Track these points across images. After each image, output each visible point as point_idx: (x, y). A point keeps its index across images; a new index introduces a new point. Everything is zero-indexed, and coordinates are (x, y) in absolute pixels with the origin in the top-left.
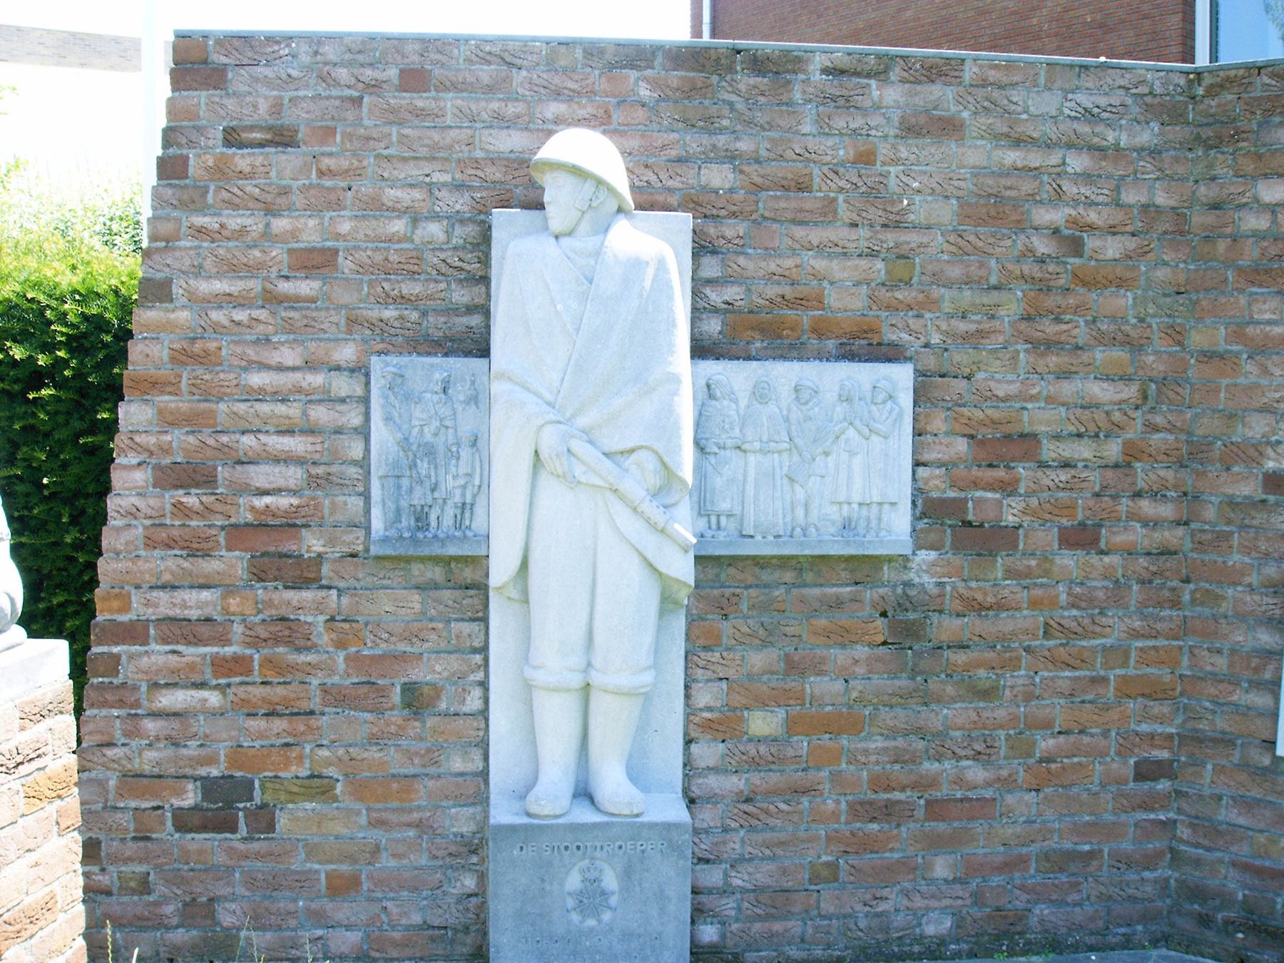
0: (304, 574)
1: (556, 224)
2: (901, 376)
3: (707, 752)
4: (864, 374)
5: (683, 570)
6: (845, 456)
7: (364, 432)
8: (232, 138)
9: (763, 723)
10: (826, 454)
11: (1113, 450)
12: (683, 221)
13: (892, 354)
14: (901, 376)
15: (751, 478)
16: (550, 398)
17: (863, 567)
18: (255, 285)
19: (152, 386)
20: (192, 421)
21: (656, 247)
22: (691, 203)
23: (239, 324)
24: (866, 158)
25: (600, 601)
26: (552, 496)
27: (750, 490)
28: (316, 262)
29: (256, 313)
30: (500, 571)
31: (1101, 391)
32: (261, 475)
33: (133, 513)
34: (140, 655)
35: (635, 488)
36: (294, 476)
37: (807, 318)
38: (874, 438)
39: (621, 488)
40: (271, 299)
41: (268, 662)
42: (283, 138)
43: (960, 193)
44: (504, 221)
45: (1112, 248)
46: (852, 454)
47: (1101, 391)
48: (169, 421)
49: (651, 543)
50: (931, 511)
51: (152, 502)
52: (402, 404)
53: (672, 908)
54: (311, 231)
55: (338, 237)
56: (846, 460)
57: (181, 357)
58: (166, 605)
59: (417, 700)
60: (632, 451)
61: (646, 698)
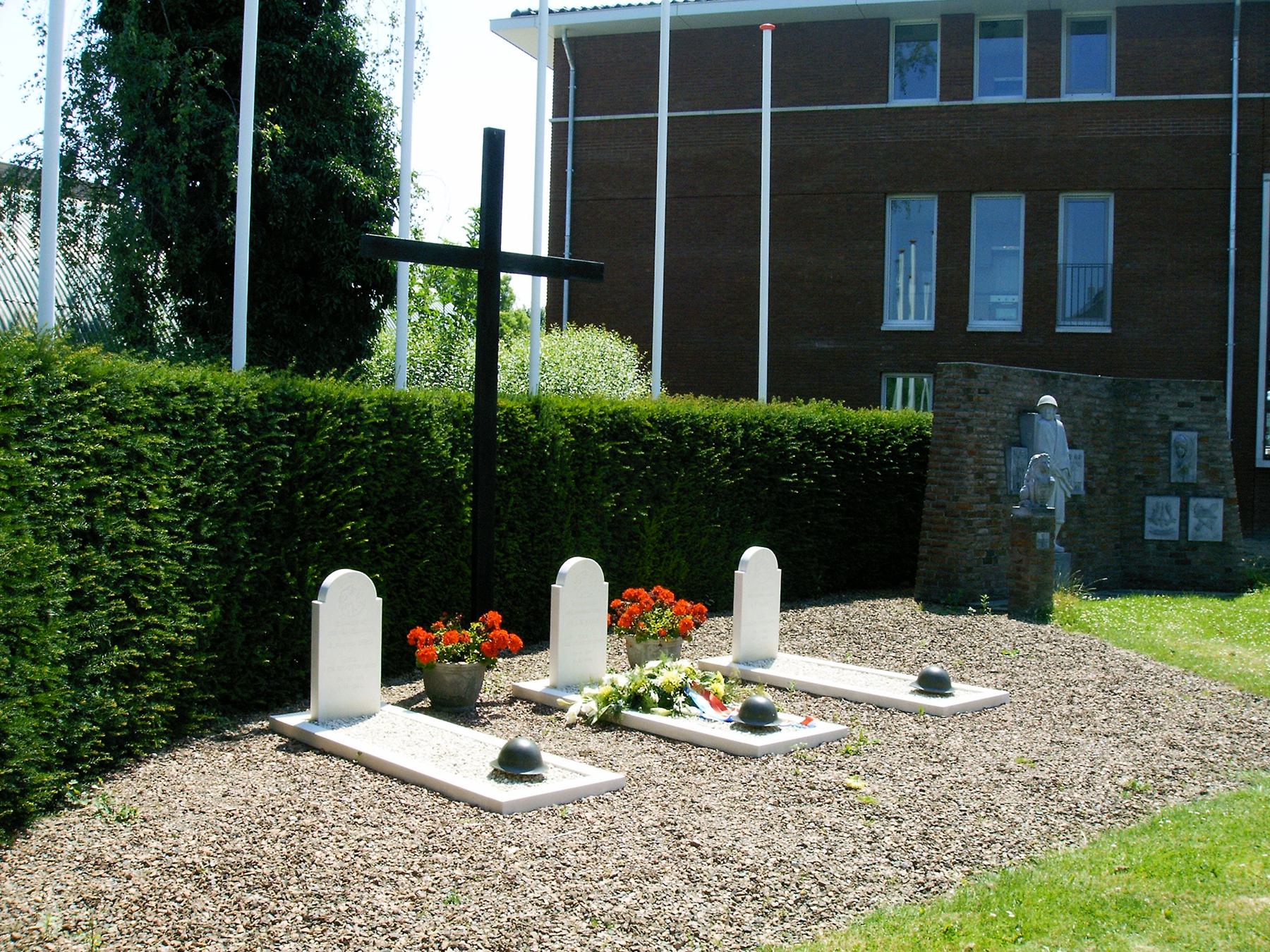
42: (987, 392)
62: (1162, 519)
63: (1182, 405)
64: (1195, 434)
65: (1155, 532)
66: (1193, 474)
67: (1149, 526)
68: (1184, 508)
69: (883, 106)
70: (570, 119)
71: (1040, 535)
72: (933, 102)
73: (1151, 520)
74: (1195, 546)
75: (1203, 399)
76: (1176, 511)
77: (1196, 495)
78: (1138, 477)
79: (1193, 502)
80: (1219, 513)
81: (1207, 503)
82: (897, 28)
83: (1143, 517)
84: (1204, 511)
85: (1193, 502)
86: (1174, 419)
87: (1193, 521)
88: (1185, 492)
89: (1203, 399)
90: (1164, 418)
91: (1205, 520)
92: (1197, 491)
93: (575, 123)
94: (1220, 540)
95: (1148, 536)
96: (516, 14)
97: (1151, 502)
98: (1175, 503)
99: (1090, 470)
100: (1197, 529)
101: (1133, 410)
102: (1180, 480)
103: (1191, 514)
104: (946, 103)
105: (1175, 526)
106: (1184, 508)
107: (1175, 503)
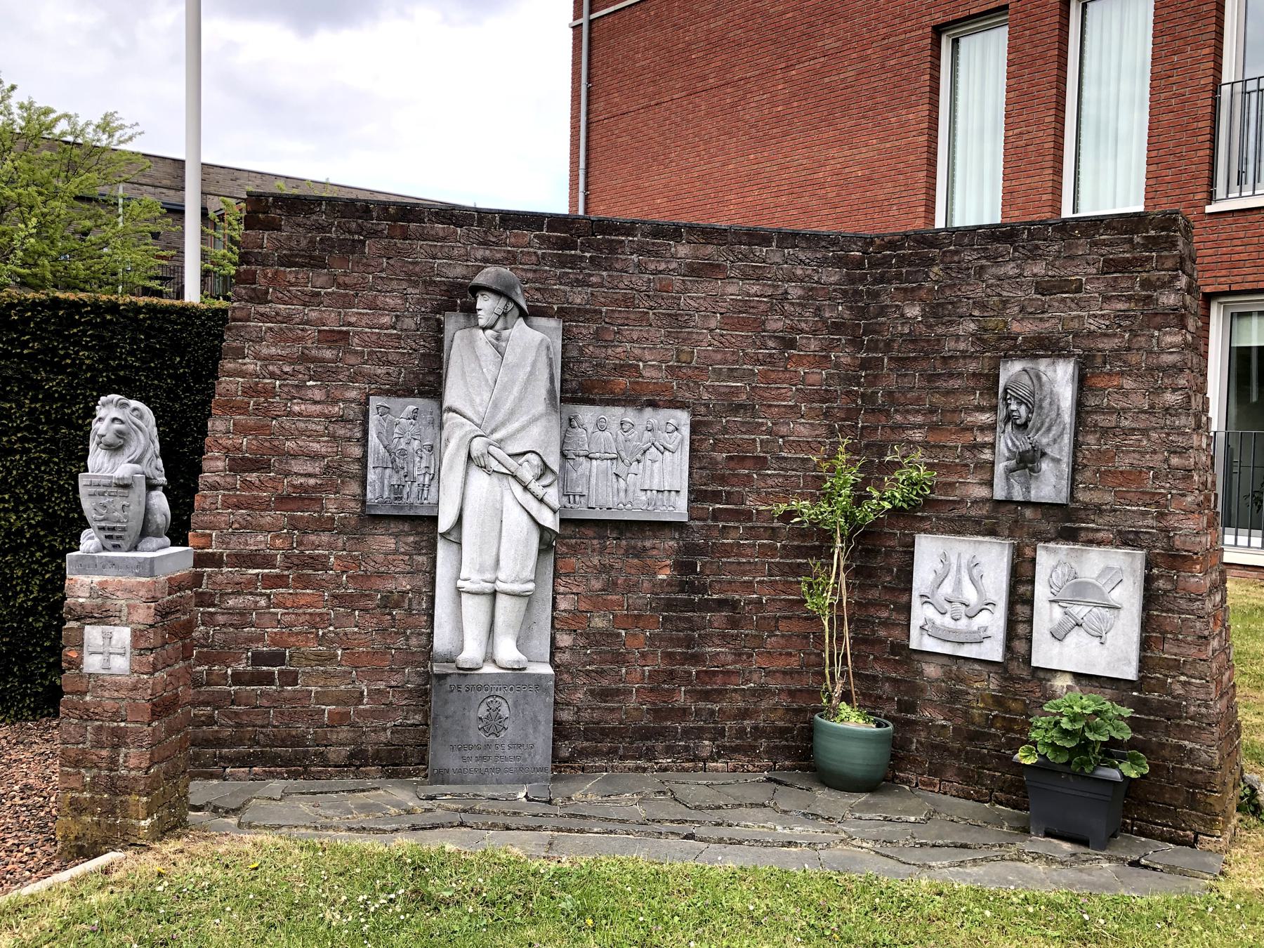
1: (482, 322)
2: (683, 418)
3: (565, 640)
5: (550, 521)
6: (649, 463)
10: (639, 461)
12: (554, 324)
15: (594, 474)
16: (478, 422)
18: (297, 349)
19: (231, 407)
20: (258, 429)
22: (562, 314)
23: (286, 373)
25: (504, 540)
26: (479, 479)
27: (593, 481)
28: (338, 338)
29: (297, 368)
30: (444, 524)
32: (297, 466)
33: (214, 487)
34: (216, 574)
35: (527, 472)
36: (316, 468)
37: (623, 382)
38: (667, 453)
39: (518, 474)
40: (304, 358)
41: (299, 578)
43: (723, 310)
44: (452, 323)
46: (654, 461)
48: (242, 430)
49: (533, 506)
51: (228, 479)
52: (392, 422)
53: (542, 728)
54: (332, 321)
55: (350, 324)
57: (250, 391)
58: (236, 545)
60: (525, 453)
61: (528, 598)
67: (920, 613)
68: (234, 320)
75: (1111, 265)
80: (1129, 596)
84: (1078, 591)
87: (1046, 615)
89: (1111, 265)
92: (1067, 523)
98: (993, 559)
105: (994, 622)
107: (993, 559)
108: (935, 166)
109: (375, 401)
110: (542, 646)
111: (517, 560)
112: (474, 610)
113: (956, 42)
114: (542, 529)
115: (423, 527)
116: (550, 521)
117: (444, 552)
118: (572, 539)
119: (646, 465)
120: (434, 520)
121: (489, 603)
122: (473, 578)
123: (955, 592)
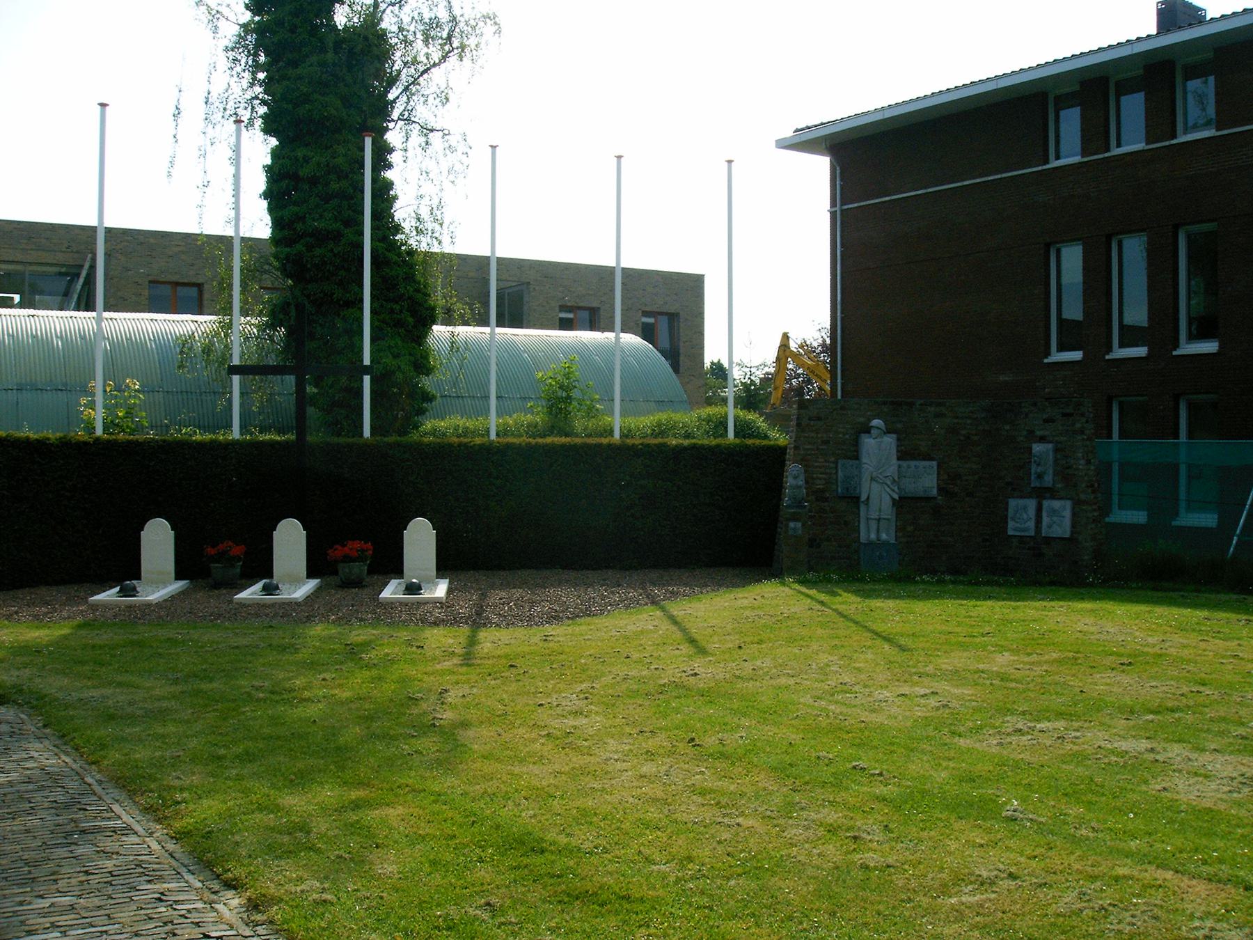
0: (826, 500)
2: (934, 463)
4: (927, 463)
5: (896, 497)
7: (836, 473)
8: (810, 419)
9: (910, 528)
11: (976, 477)
13: (932, 459)
14: (934, 463)
17: (928, 499)
21: (890, 441)
24: (927, 422)
26: (875, 486)
28: (826, 442)
30: (863, 498)
31: (974, 466)
42: (819, 419)
45: (976, 438)
47: (974, 466)
50: (940, 489)
56: (925, 479)
59: (846, 523)
62: (1021, 516)
63: (1046, 421)
64: (1050, 446)
65: (1015, 529)
66: (1048, 480)
67: (1011, 524)
68: (1039, 510)
69: (1106, 155)
70: (838, 208)
71: (792, 525)
72: (1077, 159)
73: (1013, 519)
74: (1048, 540)
75: (1064, 415)
76: (1032, 512)
77: (1053, 498)
78: (1008, 484)
79: (1046, 503)
80: (1067, 513)
81: (1056, 504)
82: (1117, 83)
83: (1006, 517)
84: (1053, 512)
85: (1046, 503)
86: (1038, 433)
87: (1045, 520)
88: (1042, 494)
89: (1064, 415)
90: (1031, 432)
91: (1055, 519)
92: (1051, 493)
93: (842, 211)
94: (1067, 535)
95: (1010, 533)
96: (797, 130)
97: (1013, 503)
98: (1031, 504)
99: (52, 445)
100: (1050, 527)
101: (1007, 427)
102: (1038, 485)
103: (1044, 514)
104: (1086, 159)
105: (1032, 524)
106: (1039, 510)
107: (1031, 504)
108: (1178, 284)
109: (840, 462)
110: (893, 534)
111: (887, 510)
112: (873, 525)
113: (1058, 252)
114: (893, 499)
115: (854, 500)
116: (896, 497)
117: (863, 508)
118: (904, 504)
119: (926, 478)
120: (858, 498)
121: (877, 522)
122: (874, 515)
123: (1021, 516)
